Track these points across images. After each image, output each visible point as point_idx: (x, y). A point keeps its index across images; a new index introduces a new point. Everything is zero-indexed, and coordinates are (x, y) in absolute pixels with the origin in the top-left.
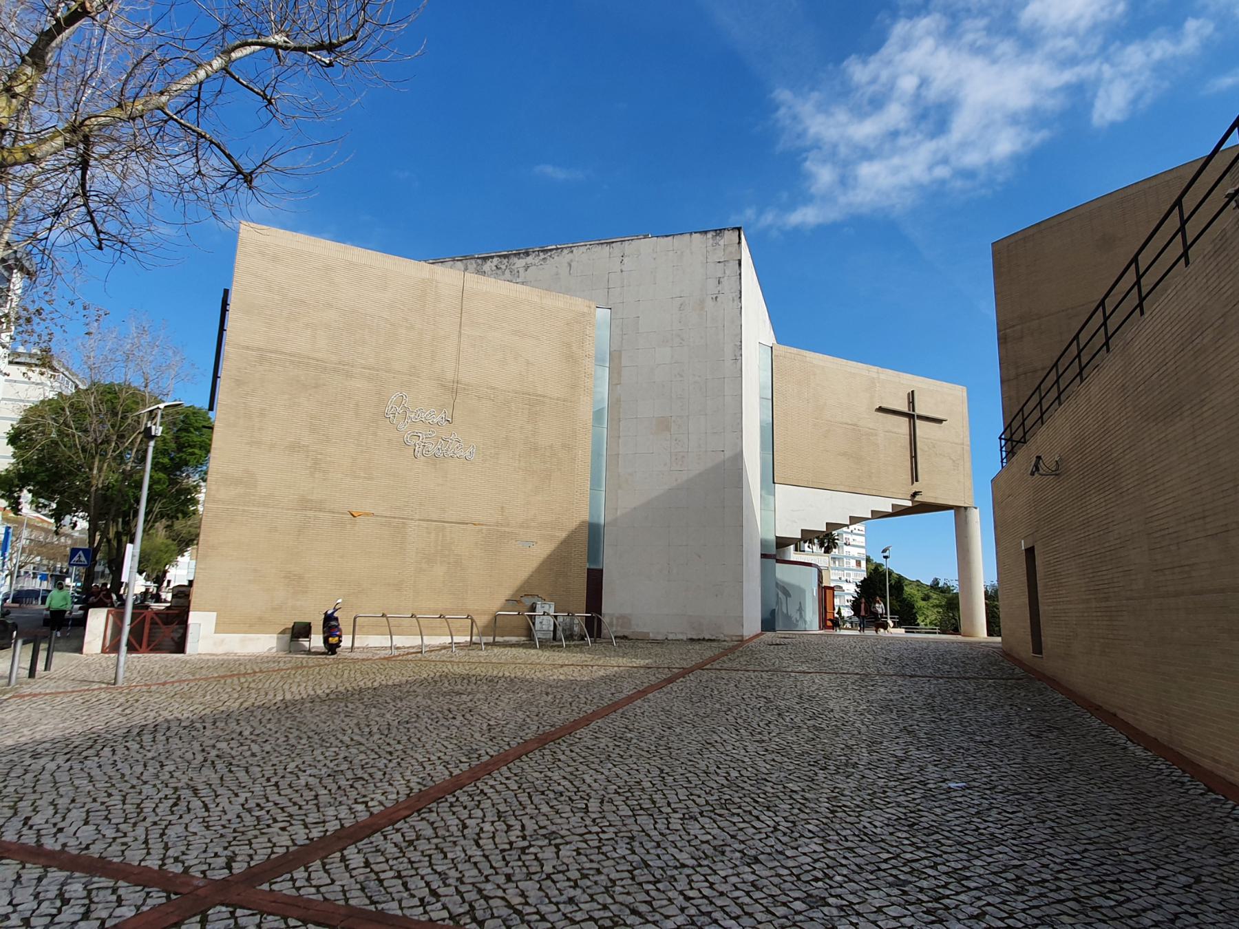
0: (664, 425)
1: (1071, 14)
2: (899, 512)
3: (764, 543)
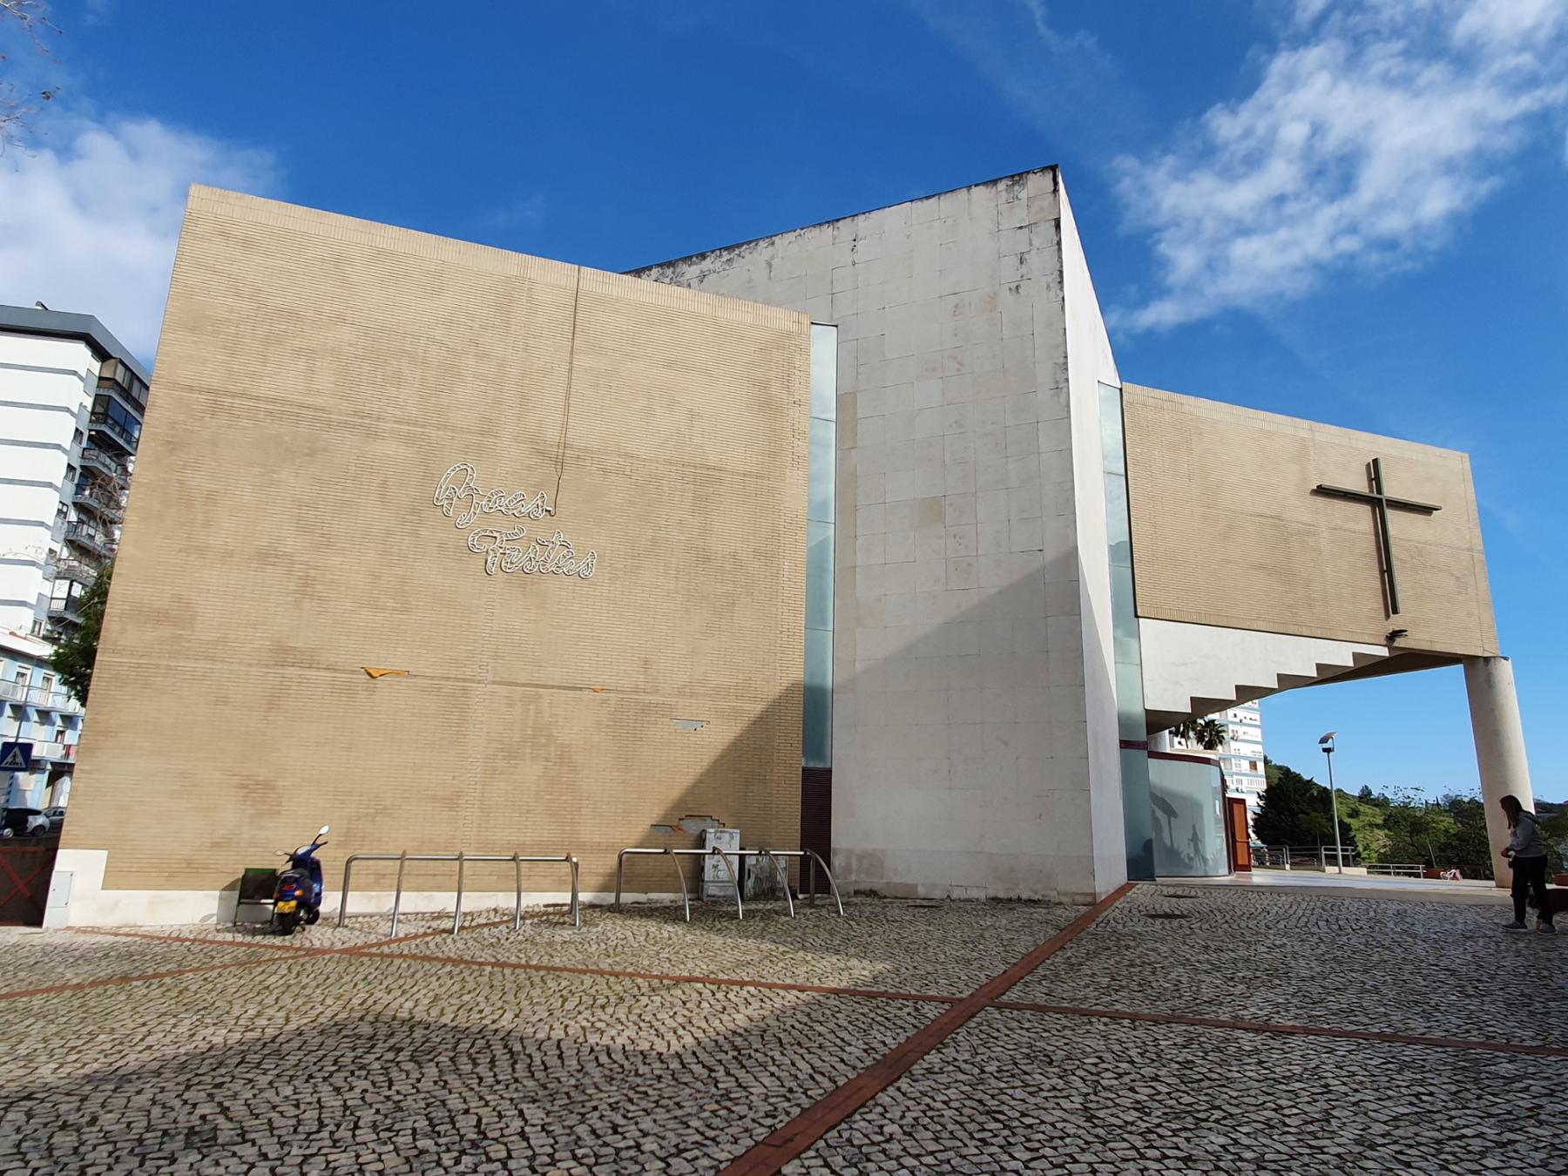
0: (932, 511)
1: (1527, 22)
2: (1366, 668)
3: (1125, 722)
